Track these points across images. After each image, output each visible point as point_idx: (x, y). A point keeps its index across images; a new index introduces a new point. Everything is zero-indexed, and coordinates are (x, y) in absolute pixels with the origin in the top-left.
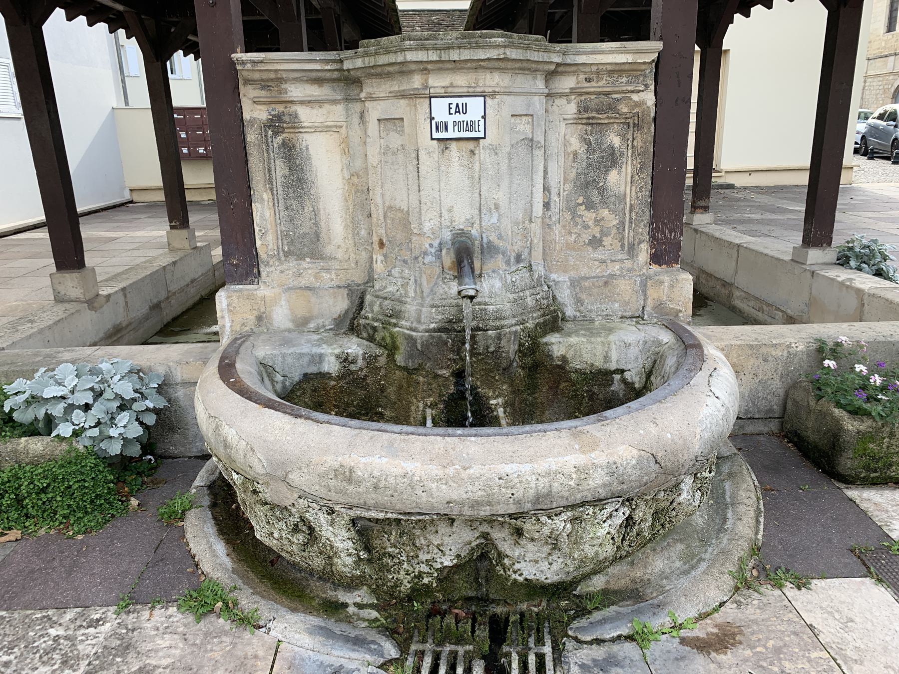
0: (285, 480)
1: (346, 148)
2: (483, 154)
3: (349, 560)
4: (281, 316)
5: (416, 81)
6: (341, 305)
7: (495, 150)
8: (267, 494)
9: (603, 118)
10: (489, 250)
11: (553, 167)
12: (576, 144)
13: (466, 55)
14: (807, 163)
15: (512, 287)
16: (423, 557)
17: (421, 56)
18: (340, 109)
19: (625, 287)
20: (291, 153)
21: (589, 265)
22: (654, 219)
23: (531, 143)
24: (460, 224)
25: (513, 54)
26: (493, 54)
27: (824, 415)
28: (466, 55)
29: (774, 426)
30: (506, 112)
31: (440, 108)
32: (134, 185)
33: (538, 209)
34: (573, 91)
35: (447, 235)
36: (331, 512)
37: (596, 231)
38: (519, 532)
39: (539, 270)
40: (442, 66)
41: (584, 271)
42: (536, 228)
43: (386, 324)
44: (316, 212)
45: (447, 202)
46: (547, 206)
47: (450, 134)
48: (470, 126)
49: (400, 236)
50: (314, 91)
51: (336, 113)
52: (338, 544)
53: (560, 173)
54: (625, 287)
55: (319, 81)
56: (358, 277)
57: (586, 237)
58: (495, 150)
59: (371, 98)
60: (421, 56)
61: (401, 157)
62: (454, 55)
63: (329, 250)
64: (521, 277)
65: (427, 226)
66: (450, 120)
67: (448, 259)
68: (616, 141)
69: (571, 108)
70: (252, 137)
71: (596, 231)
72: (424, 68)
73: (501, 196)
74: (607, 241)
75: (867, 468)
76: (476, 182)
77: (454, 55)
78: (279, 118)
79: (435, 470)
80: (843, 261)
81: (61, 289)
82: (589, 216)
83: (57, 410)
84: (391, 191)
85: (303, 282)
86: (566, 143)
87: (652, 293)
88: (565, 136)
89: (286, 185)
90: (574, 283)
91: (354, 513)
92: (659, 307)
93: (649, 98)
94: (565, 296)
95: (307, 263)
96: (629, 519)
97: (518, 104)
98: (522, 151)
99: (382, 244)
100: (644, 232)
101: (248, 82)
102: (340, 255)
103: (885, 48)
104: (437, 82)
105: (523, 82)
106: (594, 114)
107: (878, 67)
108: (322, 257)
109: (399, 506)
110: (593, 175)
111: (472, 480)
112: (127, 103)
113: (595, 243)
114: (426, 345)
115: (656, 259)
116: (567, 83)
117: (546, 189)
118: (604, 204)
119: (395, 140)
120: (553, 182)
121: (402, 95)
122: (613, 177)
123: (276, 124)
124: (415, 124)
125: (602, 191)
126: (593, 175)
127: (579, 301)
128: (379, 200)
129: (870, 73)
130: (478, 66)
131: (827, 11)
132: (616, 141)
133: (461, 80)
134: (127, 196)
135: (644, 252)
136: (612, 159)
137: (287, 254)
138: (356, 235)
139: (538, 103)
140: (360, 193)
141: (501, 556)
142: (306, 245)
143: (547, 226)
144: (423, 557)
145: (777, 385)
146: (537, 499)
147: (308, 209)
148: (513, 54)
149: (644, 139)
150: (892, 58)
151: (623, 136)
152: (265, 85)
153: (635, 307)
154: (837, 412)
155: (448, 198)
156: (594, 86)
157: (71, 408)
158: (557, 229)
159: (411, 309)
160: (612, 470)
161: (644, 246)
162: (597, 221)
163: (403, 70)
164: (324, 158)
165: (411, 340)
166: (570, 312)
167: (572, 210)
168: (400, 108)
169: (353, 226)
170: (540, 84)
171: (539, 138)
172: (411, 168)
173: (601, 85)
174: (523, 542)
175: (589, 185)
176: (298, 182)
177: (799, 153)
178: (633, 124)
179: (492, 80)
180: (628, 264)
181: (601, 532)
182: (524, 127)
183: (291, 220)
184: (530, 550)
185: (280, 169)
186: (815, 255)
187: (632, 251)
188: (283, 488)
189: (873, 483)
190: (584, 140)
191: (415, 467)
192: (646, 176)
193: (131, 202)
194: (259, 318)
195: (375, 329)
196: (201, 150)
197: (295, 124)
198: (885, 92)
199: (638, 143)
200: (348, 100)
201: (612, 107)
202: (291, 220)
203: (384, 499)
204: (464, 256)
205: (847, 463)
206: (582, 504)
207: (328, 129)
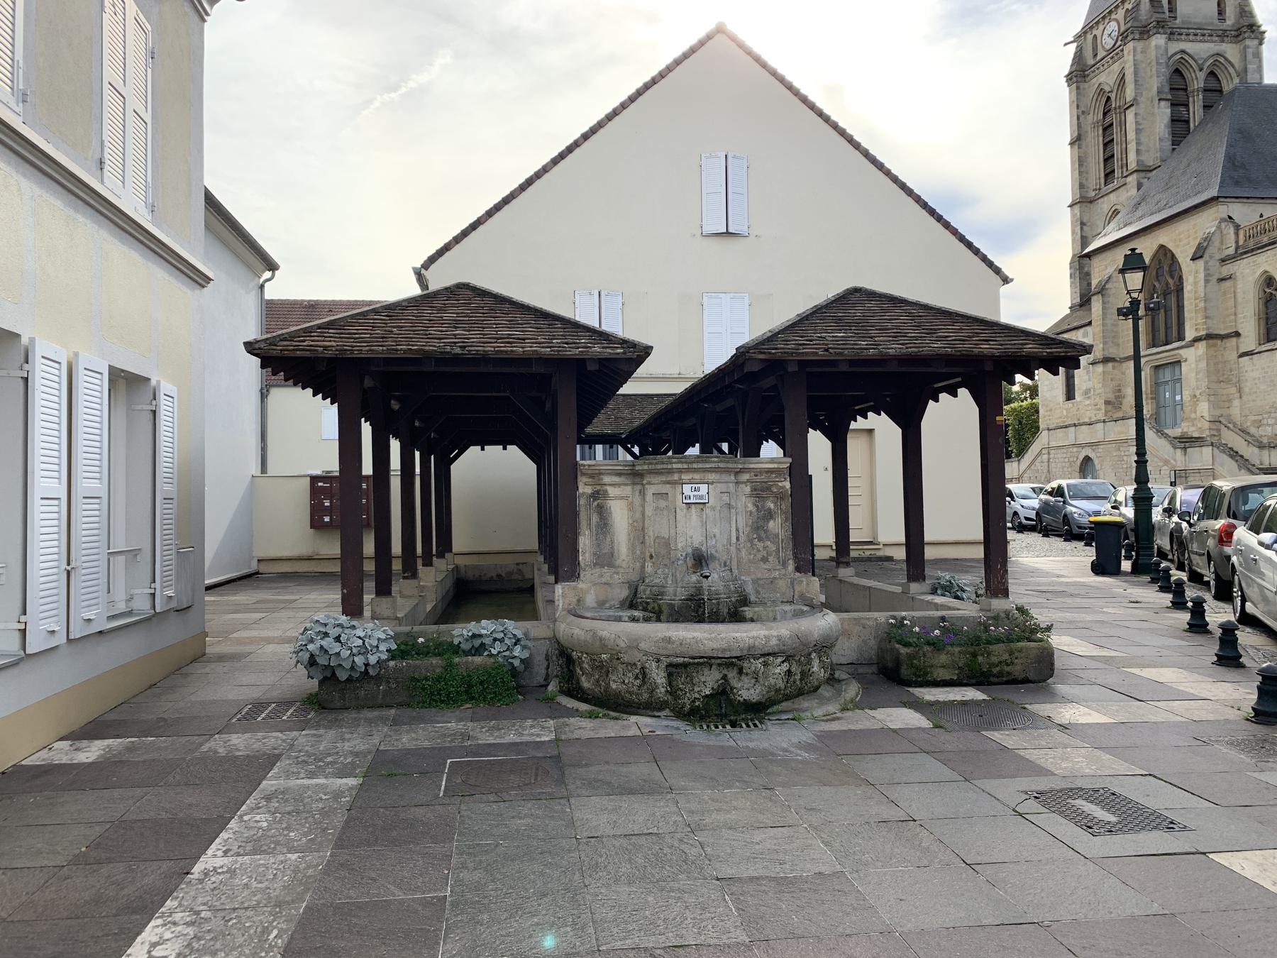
0: (637, 648)
1: (631, 508)
2: (708, 511)
3: (663, 690)
4: (590, 600)
5: (676, 477)
6: (624, 593)
7: (713, 509)
8: (626, 658)
9: (764, 494)
10: (713, 557)
11: (740, 518)
12: (751, 507)
13: (700, 466)
14: (979, 535)
15: (722, 579)
16: (697, 689)
17: (680, 466)
18: (629, 488)
19: (782, 584)
20: (602, 512)
21: (762, 571)
22: (795, 546)
23: (729, 506)
24: (696, 544)
25: (721, 465)
26: (713, 465)
27: (893, 649)
28: (700, 466)
29: (874, 669)
30: (718, 490)
31: (687, 489)
32: (262, 555)
33: (734, 540)
34: (748, 481)
35: (690, 550)
36: (658, 661)
37: (764, 553)
38: (740, 671)
39: (736, 572)
40: (688, 470)
41: (759, 575)
42: (733, 549)
43: (655, 600)
44: (612, 541)
45: (690, 533)
46: (738, 539)
47: (692, 501)
48: (701, 497)
49: (663, 552)
50: (616, 479)
51: (627, 490)
52: (659, 681)
53: (742, 521)
54: (782, 584)
55: (619, 474)
56: (634, 577)
57: (759, 556)
58: (713, 509)
59: (649, 483)
60: (680, 466)
61: (665, 512)
62: (695, 466)
63: (618, 562)
64: (726, 574)
65: (680, 546)
66: (692, 494)
67: (690, 562)
68: (772, 506)
69: (748, 489)
70: (582, 502)
71: (764, 553)
72: (680, 471)
73: (716, 531)
74: (771, 559)
75: (915, 674)
76: (704, 524)
77: (695, 466)
78: (598, 492)
79: (706, 635)
80: (934, 591)
81: (378, 610)
82: (760, 545)
83: (487, 641)
84: (658, 527)
85: (604, 580)
86: (746, 507)
87: (797, 588)
88: (745, 502)
89: (598, 526)
90: (755, 582)
91: (668, 660)
92: (802, 596)
93: (787, 485)
94: (749, 589)
95: (605, 569)
96: (789, 671)
97: (722, 487)
98: (725, 510)
99: (651, 557)
100: (790, 553)
101: (583, 474)
102: (624, 565)
103: (1067, 417)
104: (685, 477)
105: (725, 477)
106: (760, 492)
107: (1059, 438)
108: (614, 566)
109: (691, 653)
110: (761, 523)
111: (722, 639)
112: (264, 468)
113: (765, 560)
114: (680, 608)
115: (798, 569)
116: (746, 477)
117: (737, 530)
118: (768, 539)
119: (662, 504)
120: (740, 527)
121: (668, 483)
122: (771, 524)
123: (595, 495)
124: (675, 496)
125: (766, 531)
126: (761, 523)
127: (758, 592)
128: (651, 533)
129: (1053, 444)
130: (705, 470)
131: (900, 430)
132: (772, 506)
133: (697, 476)
134: (254, 566)
135: (791, 566)
136: (770, 515)
137: (595, 565)
138: (633, 553)
139: (732, 487)
140: (639, 531)
141: (732, 688)
142: (605, 559)
143: (738, 550)
144: (697, 689)
145: (873, 643)
146: (749, 649)
147: (608, 539)
148: (721, 465)
149: (786, 505)
150: (1072, 429)
151: (775, 504)
152: (592, 476)
153: (789, 596)
154: (897, 646)
155: (691, 532)
156: (759, 478)
157: (495, 640)
158: (744, 552)
159: (670, 590)
160: (779, 638)
161: (791, 562)
162: (765, 548)
163: (670, 471)
164: (620, 514)
165: (671, 606)
166: (753, 598)
167: (751, 541)
168: (667, 489)
169: (632, 548)
170: (733, 478)
171: (733, 503)
172: (672, 517)
173: (763, 477)
174: (743, 677)
175: (759, 528)
176: (604, 524)
177: (976, 531)
178: (780, 497)
179: (712, 477)
180: (783, 572)
181: (777, 671)
182: (725, 498)
183: (599, 545)
184: (747, 681)
185: (595, 518)
186: (914, 587)
187: (784, 564)
188: (636, 652)
189: (921, 685)
190: (755, 505)
191: (697, 634)
192: (789, 524)
193: (257, 573)
194: (579, 601)
195: (648, 603)
196: (327, 519)
197: (605, 495)
198: (1071, 466)
199: (783, 507)
200: (634, 484)
201: (769, 489)
202: (599, 545)
203: (684, 649)
204: (700, 560)
205: (905, 672)
206: (769, 654)
207: (622, 498)
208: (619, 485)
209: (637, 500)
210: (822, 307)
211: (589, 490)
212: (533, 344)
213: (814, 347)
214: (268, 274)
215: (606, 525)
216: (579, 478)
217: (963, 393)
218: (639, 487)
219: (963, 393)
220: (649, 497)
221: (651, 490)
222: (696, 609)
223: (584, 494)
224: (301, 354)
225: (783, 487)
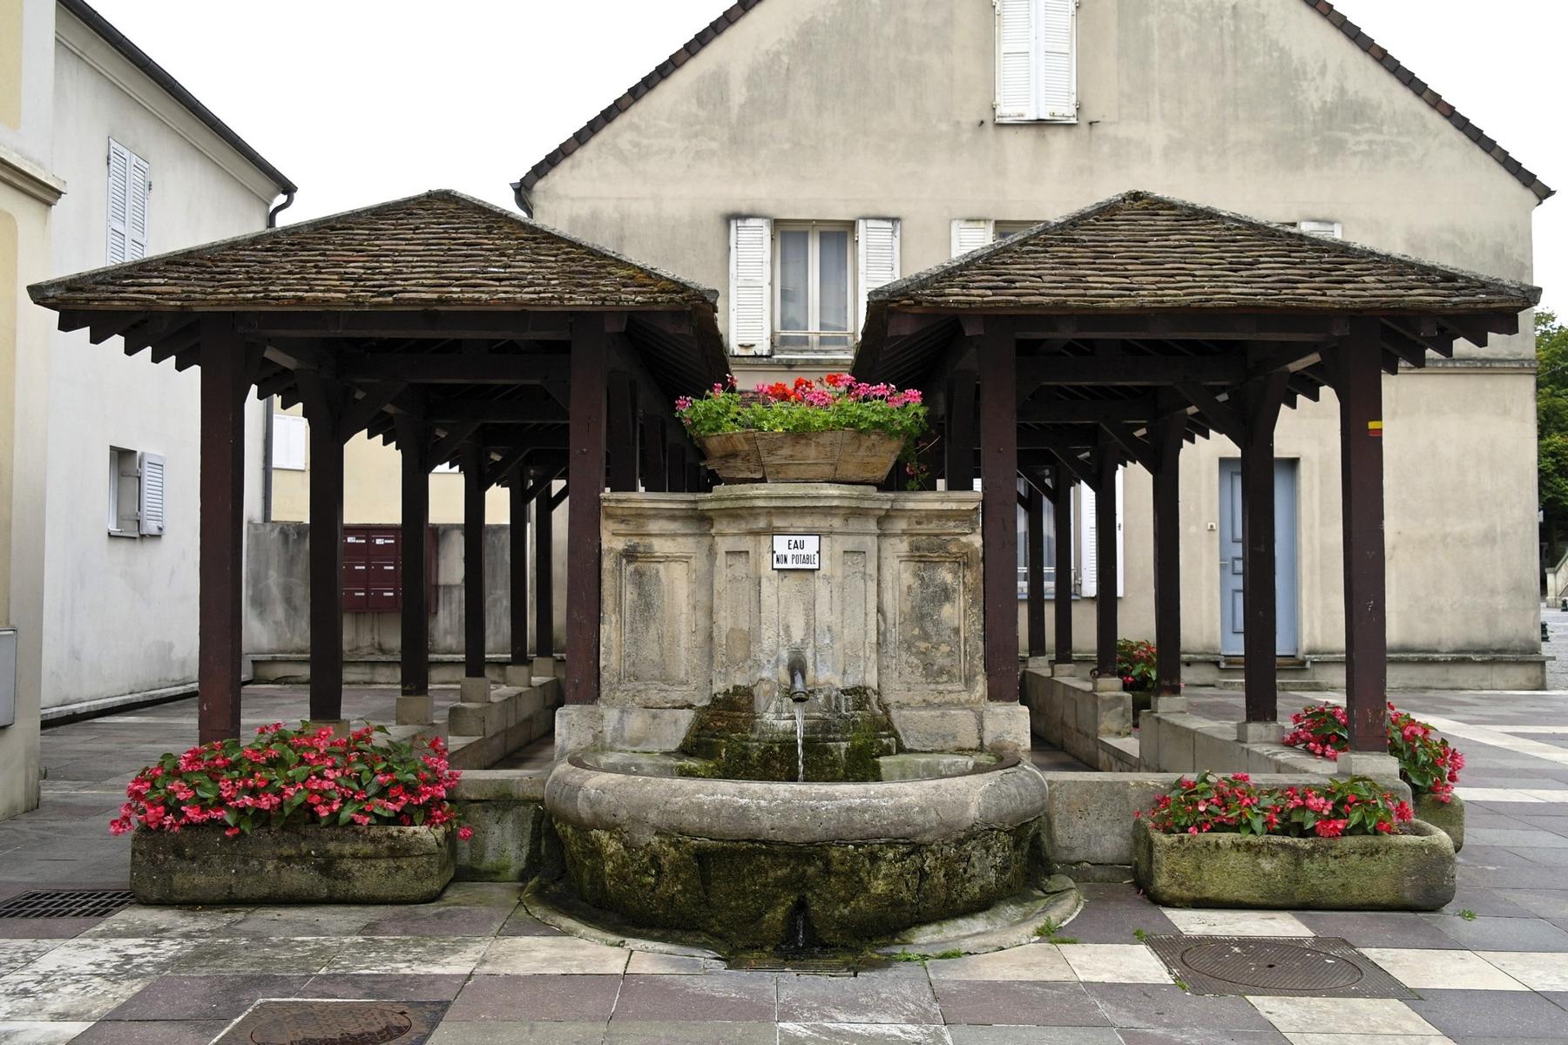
5: (762, 523)
18: (691, 541)
30: (839, 549)
31: (781, 544)
34: (904, 533)
47: (789, 565)
48: (807, 559)
66: (789, 554)
68: (949, 578)
69: (903, 546)
70: (607, 564)
93: (977, 541)
101: (609, 516)
105: (855, 525)
123: (630, 555)
125: (937, 623)
131: (346, 446)
132: (949, 578)
135: (981, 688)
136: (945, 594)
139: (870, 543)
149: (973, 576)
156: (927, 528)
168: (747, 543)
173: (932, 527)
176: (646, 606)
178: (962, 561)
185: (630, 594)
186: (1254, 729)
190: (915, 575)
192: (977, 611)
199: (969, 578)
200: (701, 535)
201: (942, 547)
208: (674, 535)
209: (699, 563)
210: (1089, 215)
211: (620, 544)
212: (1372, 289)
213: (1043, 284)
214: (281, 199)
215: (648, 606)
216: (604, 523)
217: (195, 371)
218: (706, 541)
219: (195, 371)
220: (721, 559)
221: (723, 545)
222: (813, 758)
223: (611, 550)
224: (253, 321)
225: (968, 545)
